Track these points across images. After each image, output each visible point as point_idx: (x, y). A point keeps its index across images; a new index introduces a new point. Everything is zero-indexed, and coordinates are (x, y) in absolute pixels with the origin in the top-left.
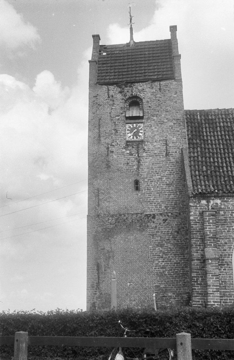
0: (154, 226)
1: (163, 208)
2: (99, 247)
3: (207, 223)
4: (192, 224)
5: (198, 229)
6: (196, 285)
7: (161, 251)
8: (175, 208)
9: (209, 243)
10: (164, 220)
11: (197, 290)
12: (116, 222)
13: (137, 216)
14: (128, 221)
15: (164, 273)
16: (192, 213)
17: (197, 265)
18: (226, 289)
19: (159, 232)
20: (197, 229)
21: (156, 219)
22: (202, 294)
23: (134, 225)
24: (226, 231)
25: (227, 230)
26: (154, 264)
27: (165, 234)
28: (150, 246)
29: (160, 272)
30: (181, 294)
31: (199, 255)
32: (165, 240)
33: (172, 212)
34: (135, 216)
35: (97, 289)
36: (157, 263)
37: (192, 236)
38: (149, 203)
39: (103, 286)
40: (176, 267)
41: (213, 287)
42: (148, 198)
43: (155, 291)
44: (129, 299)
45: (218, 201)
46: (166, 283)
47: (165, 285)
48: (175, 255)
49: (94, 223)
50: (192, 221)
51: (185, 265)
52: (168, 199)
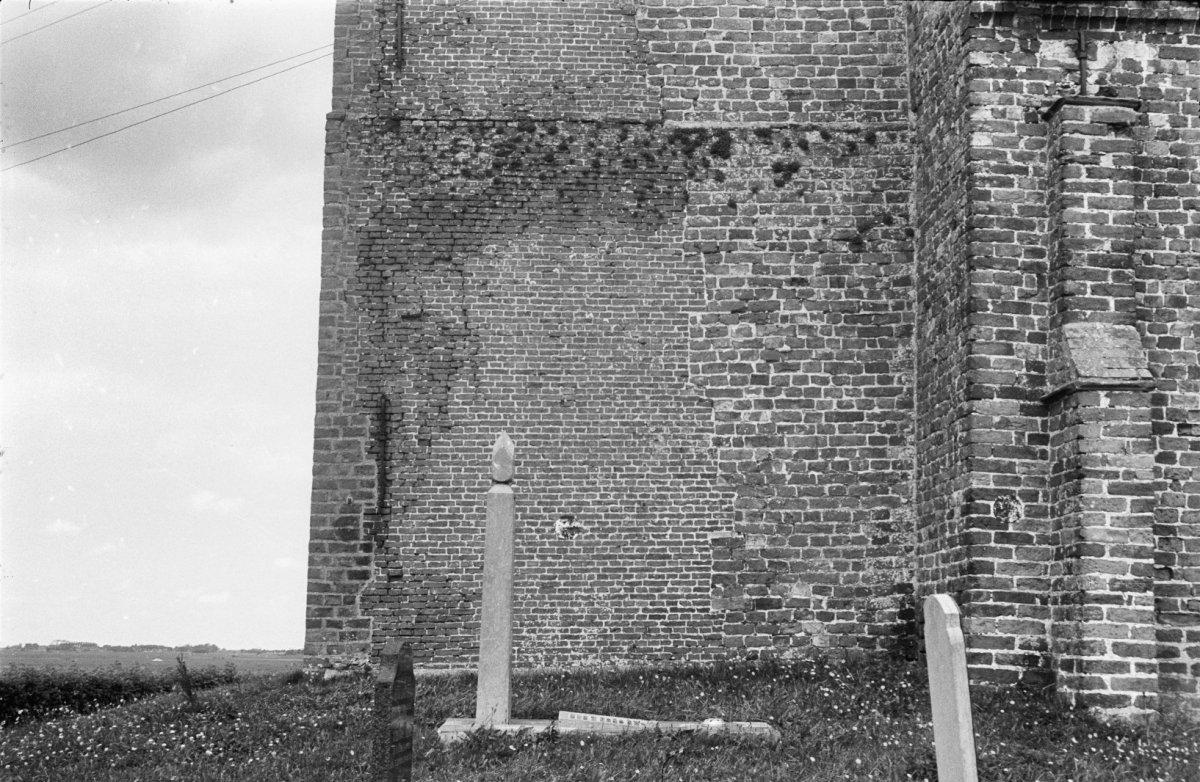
0: (718, 201)
1: (772, 99)
2: (390, 300)
3: (1084, 173)
4: (983, 179)
5: (1015, 206)
6: (993, 544)
7: (758, 343)
8: (845, 102)
9: (1094, 292)
10: (777, 168)
11: (996, 575)
12: (497, 166)
13: (623, 138)
14: (572, 162)
15: (769, 471)
16: (982, 114)
17: (1005, 423)
18: (1172, 575)
19: (747, 235)
20: (1009, 211)
21: (734, 159)
22: (1030, 599)
23: (604, 190)
24: (1182, 231)
25: (1190, 223)
26: (713, 419)
27: (782, 247)
28: (691, 314)
29: (744, 466)
30: (861, 592)
31: (1015, 364)
32: (779, 284)
33: (825, 125)
34: (610, 136)
35: (375, 547)
36: (731, 409)
37: (981, 250)
38: (695, 68)
39: (408, 533)
40: (839, 441)
41: (1115, 559)
42: (693, 36)
43: (713, 572)
44: (558, 614)
45: (1141, 51)
46: (781, 529)
47: (772, 541)
48: (834, 369)
49: (368, 162)
50: (981, 162)
51: (889, 429)
52: (806, 49)
